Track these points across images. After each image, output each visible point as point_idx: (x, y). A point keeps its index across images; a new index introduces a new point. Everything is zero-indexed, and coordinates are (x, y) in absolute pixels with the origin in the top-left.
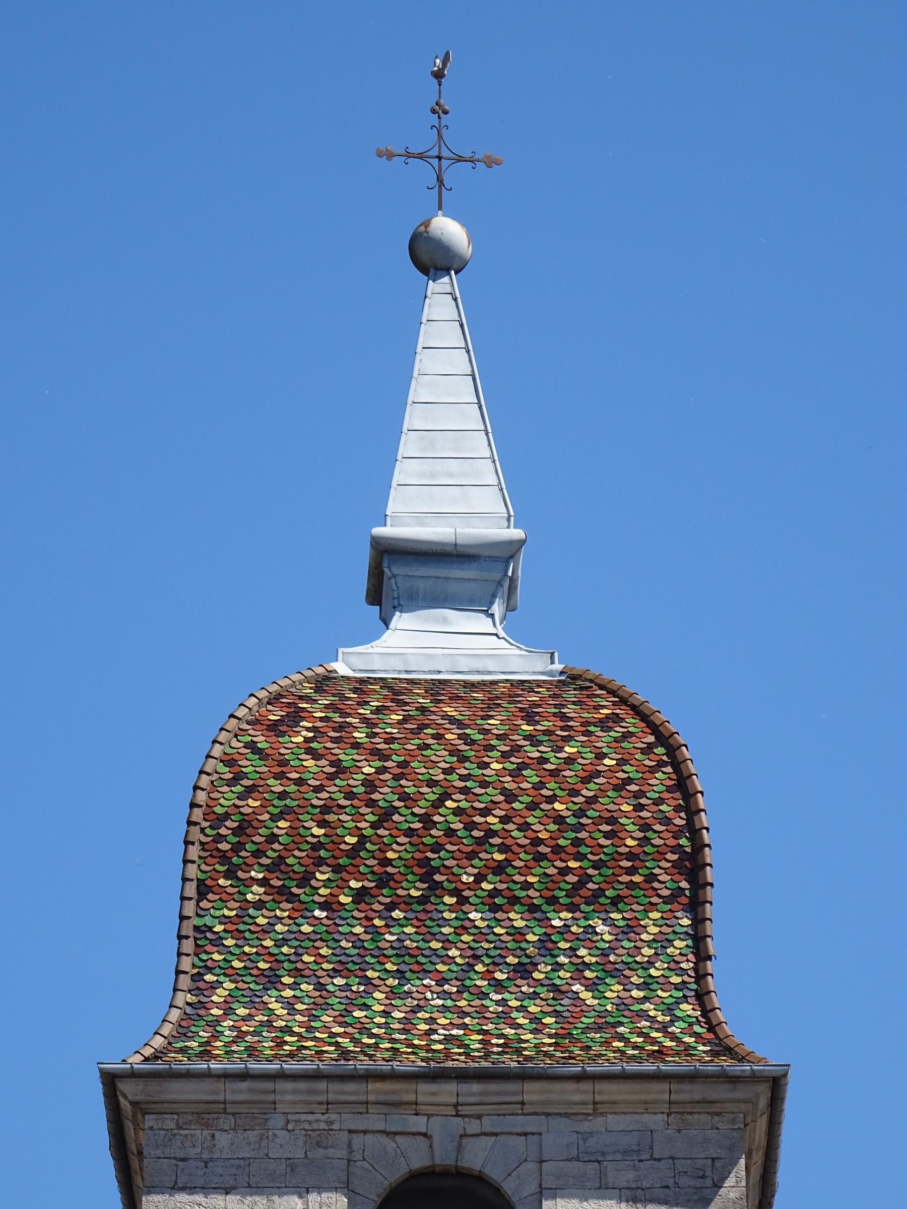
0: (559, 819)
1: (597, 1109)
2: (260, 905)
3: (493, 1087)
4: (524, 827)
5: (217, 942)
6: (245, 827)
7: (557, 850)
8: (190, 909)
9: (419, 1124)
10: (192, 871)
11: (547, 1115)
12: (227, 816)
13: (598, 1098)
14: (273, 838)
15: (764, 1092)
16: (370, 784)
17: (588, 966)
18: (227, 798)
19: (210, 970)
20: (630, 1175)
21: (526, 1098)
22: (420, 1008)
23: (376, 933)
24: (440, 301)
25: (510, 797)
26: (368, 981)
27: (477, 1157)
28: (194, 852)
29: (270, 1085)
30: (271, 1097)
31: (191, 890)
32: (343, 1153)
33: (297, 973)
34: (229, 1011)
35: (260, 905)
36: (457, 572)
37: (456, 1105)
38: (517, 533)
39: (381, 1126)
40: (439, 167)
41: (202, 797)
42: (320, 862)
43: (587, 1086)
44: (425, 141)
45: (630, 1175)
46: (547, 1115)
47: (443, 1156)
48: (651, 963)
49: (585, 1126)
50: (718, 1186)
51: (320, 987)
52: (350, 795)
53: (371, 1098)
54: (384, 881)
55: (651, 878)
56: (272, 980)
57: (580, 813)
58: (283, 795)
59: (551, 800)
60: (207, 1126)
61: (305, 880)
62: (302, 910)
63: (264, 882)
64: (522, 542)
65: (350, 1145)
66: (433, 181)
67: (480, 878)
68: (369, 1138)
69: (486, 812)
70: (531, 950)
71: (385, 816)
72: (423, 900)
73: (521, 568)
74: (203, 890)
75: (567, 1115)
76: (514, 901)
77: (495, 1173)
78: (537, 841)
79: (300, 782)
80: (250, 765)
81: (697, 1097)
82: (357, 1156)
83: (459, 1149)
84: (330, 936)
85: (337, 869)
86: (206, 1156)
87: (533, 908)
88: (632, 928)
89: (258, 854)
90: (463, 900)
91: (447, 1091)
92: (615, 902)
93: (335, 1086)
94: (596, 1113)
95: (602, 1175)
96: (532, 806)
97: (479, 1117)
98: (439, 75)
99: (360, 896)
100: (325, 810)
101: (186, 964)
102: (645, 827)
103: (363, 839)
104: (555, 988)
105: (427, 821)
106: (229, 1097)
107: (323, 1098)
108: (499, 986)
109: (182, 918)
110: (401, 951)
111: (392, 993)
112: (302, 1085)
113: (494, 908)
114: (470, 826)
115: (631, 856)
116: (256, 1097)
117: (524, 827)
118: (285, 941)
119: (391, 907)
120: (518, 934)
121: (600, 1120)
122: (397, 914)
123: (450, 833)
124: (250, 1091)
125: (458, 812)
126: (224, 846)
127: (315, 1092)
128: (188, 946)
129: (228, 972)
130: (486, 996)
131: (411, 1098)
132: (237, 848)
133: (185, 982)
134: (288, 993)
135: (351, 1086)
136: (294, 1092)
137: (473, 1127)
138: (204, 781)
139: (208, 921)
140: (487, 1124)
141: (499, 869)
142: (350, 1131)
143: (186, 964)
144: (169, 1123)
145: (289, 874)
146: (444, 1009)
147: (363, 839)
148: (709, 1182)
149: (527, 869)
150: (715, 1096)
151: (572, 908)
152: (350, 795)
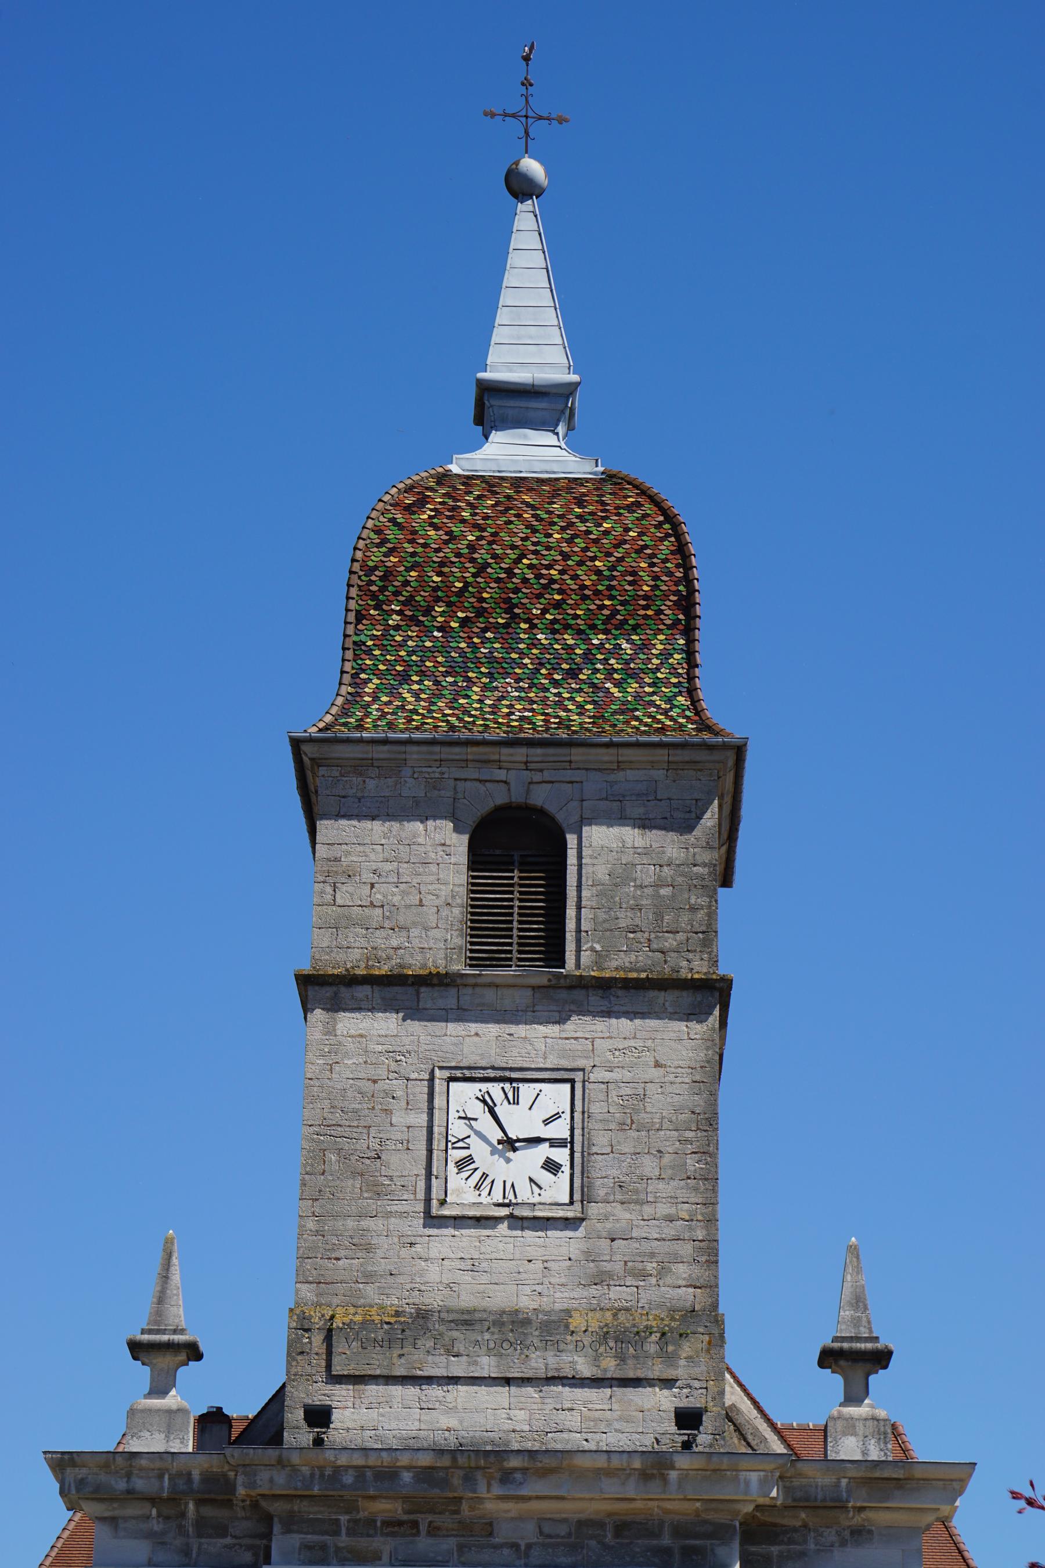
0: (598, 572)
1: (620, 766)
2: (397, 628)
3: (551, 751)
4: (575, 577)
5: (369, 652)
6: (388, 575)
7: (597, 593)
8: (350, 629)
9: (501, 775)
10: (352, 605)
11: (587, 769)
12: (376, 568)
13: (620, 759)
14: (406, 583)
15: (731, 758)
16: (472, 547)
17: (616, 671)
18: (376, 556)
19: (363, 671)
20: (641, 810)
21: (573, 758)
22: (503, 698)
23: (475, 647)
24: (526, 219)
25: (566, 557)
26: (468, 680)
27: (540, 797)
28: (354, 592)
29: (402, 748)
30: (403, 756)
31: (352, 617)
32: (450, 794)
33: (421, 673)
34: (376, 699)
35: (397, 628)
36: (533, 404)
37: (526, 763)
38: (575, 378)
39: (476, 776)
40: (527, 123)
41: (359, 555)
42: (438, 599)
43: (613, 751)
44: (516, 105)
45: (641, 810)
46: (587, 769)
47: (517, 796)
48: (658, 669)
49: (612, 777)
50: (699, 818)
51: (437, 683)
52: (458, 555)
53: (469, 757)
54: (480, 612)
55: (659, 612)
56: (404, 678)
57: (612, 568)
58: (413, 554)
59: (593, 559)
60: (361, 775)
61: (428, 611)
62: (426, 632)
63: (400, 613)
64: (578, 384)
65: (455, 789)
66: (522, 134)
67: (544, 611)
68: (468, 783)
69: (549, 567)
70: (578, 660)
71: (482, 569)
72: (506, 626)
73: (577, 401)
74: (360, 617)
75: (599, 770)
76: (567, 627)
77: (551, 808)
78: (583, 587)
79: (425, 546)
80: (392, 534)
81: (687, 759)
82: (460, 796)
83: (528, 792)
84: (445, 649)
85: (449, 604)
86: (359, 794)
87: (580, 632)
88: (645, 646)
89: (397, 593)
90: (533, 626)
91: (520, 753)
92: (635, 628)
93: (446, 749)
94: (619, 769)
95: (622, 810)
96: (580, 563)
97: (541, 770)
98: (527, 59)
99: (464, 622)
100: (442, 564)
101: (348, 666)
102: (656, 578)
103: (467, 585)
104: (593, 685)
105: (510, 572)
106: (375, 756)
107: (438, 757)
108: (556, 683)
109: (346, 636)
110: (491, 659)
111: (485, 688)
112: (424, 748)
113: (554, 632)
114: (539, 576)
115: (646, 597)
116: (392, 756)
117: (575, 577)
118: (414, 652)
119: (485, 630)
120: (569, 649)
121: (621, 773)
122: (489, 635)
123: (525, 581)
124: (389, 752)
125: (530, 567)
126: (374, 588)
127: (431, 753)
128: (349, 655)
129: (379, 675)
130: (547, 690)
131: (496, 757)
132: (383, 589)
133: (347, 678)
134: (416, 687)
135: (457, 750)
136: (419, 753)
137: (537, 777)
138: (361, 544)
139: (363, 638)
140: (547, 775)
141: (558, 605)
142: (456, 779)
143: (348, 666)
144: (335, 772)
145: (417, 607)
146: (519, 699)
147: (467, 585)
148: (693, 815)
149: (575, 606)
150: (698, 759)
151: (606, 632)
152: (458, 555)
